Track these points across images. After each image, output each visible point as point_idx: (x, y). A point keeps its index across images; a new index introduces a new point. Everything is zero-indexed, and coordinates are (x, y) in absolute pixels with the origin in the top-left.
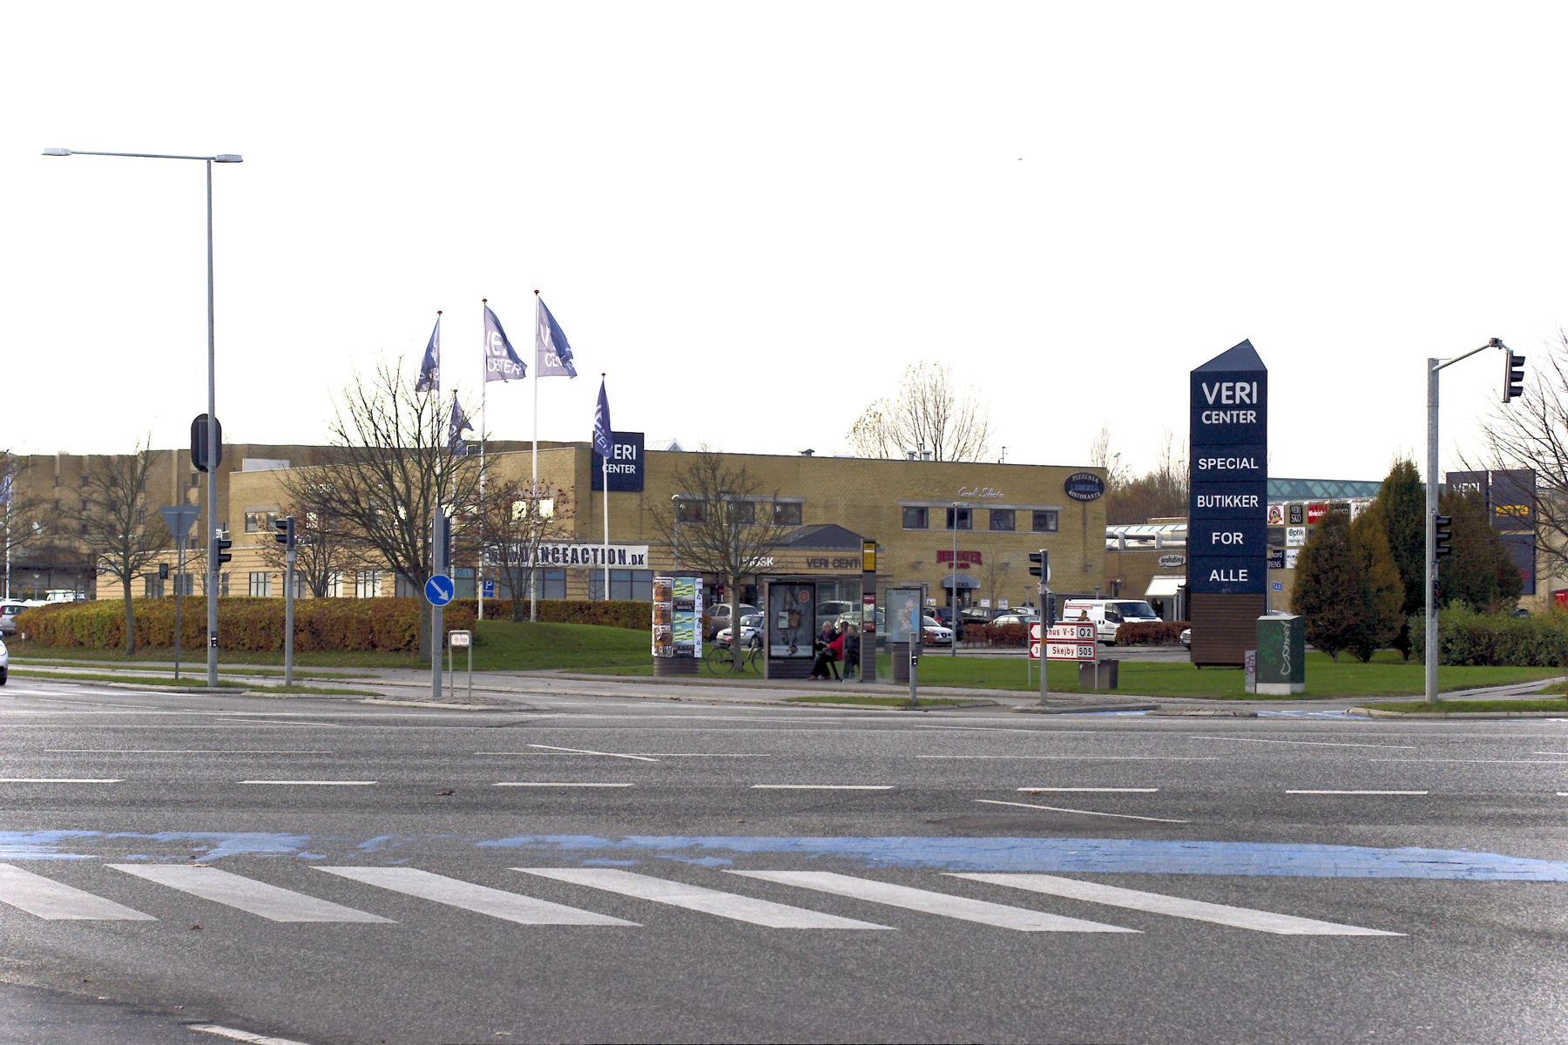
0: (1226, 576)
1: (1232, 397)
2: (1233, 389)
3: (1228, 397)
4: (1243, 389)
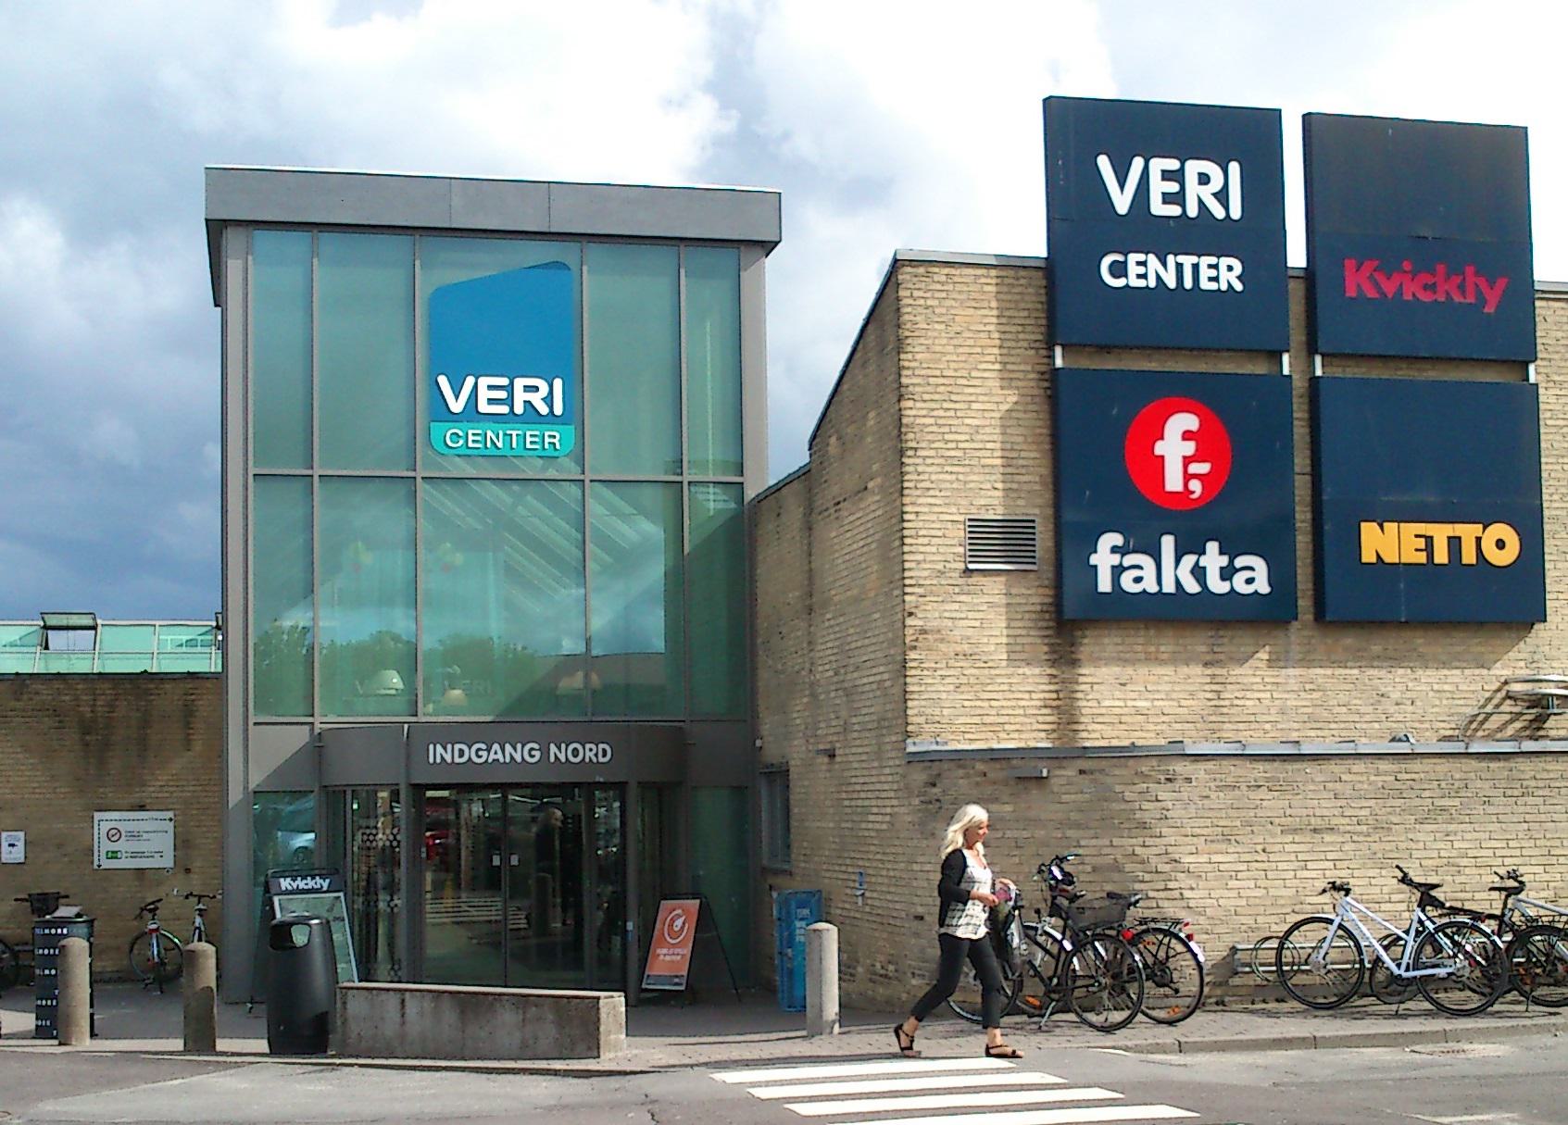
0: (1455, 543)
1: (1178, 198)
2: (1177, 176)
3: (1167, 198)
4: (1204, 179)
